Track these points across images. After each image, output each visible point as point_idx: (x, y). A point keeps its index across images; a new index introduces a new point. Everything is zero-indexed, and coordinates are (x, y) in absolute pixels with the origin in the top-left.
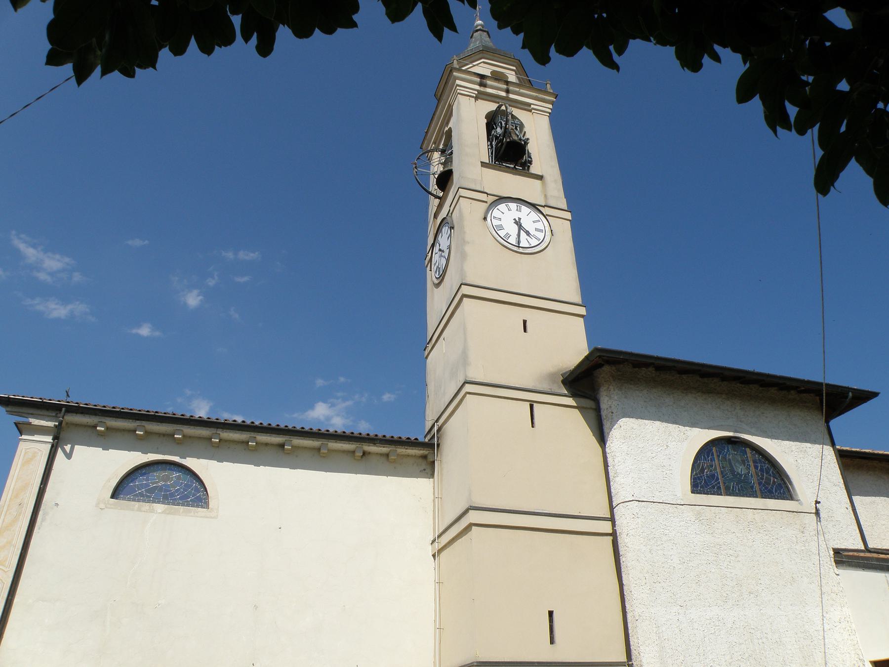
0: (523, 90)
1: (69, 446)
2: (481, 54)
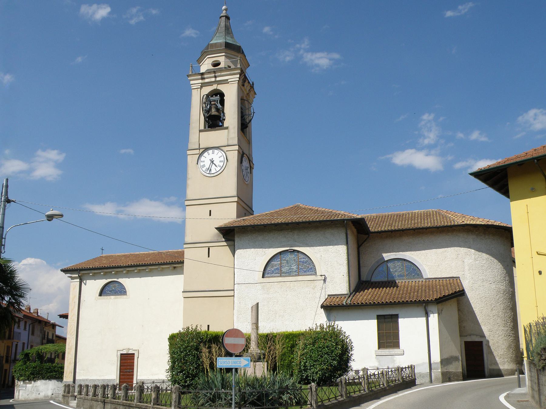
1: (85, 281)
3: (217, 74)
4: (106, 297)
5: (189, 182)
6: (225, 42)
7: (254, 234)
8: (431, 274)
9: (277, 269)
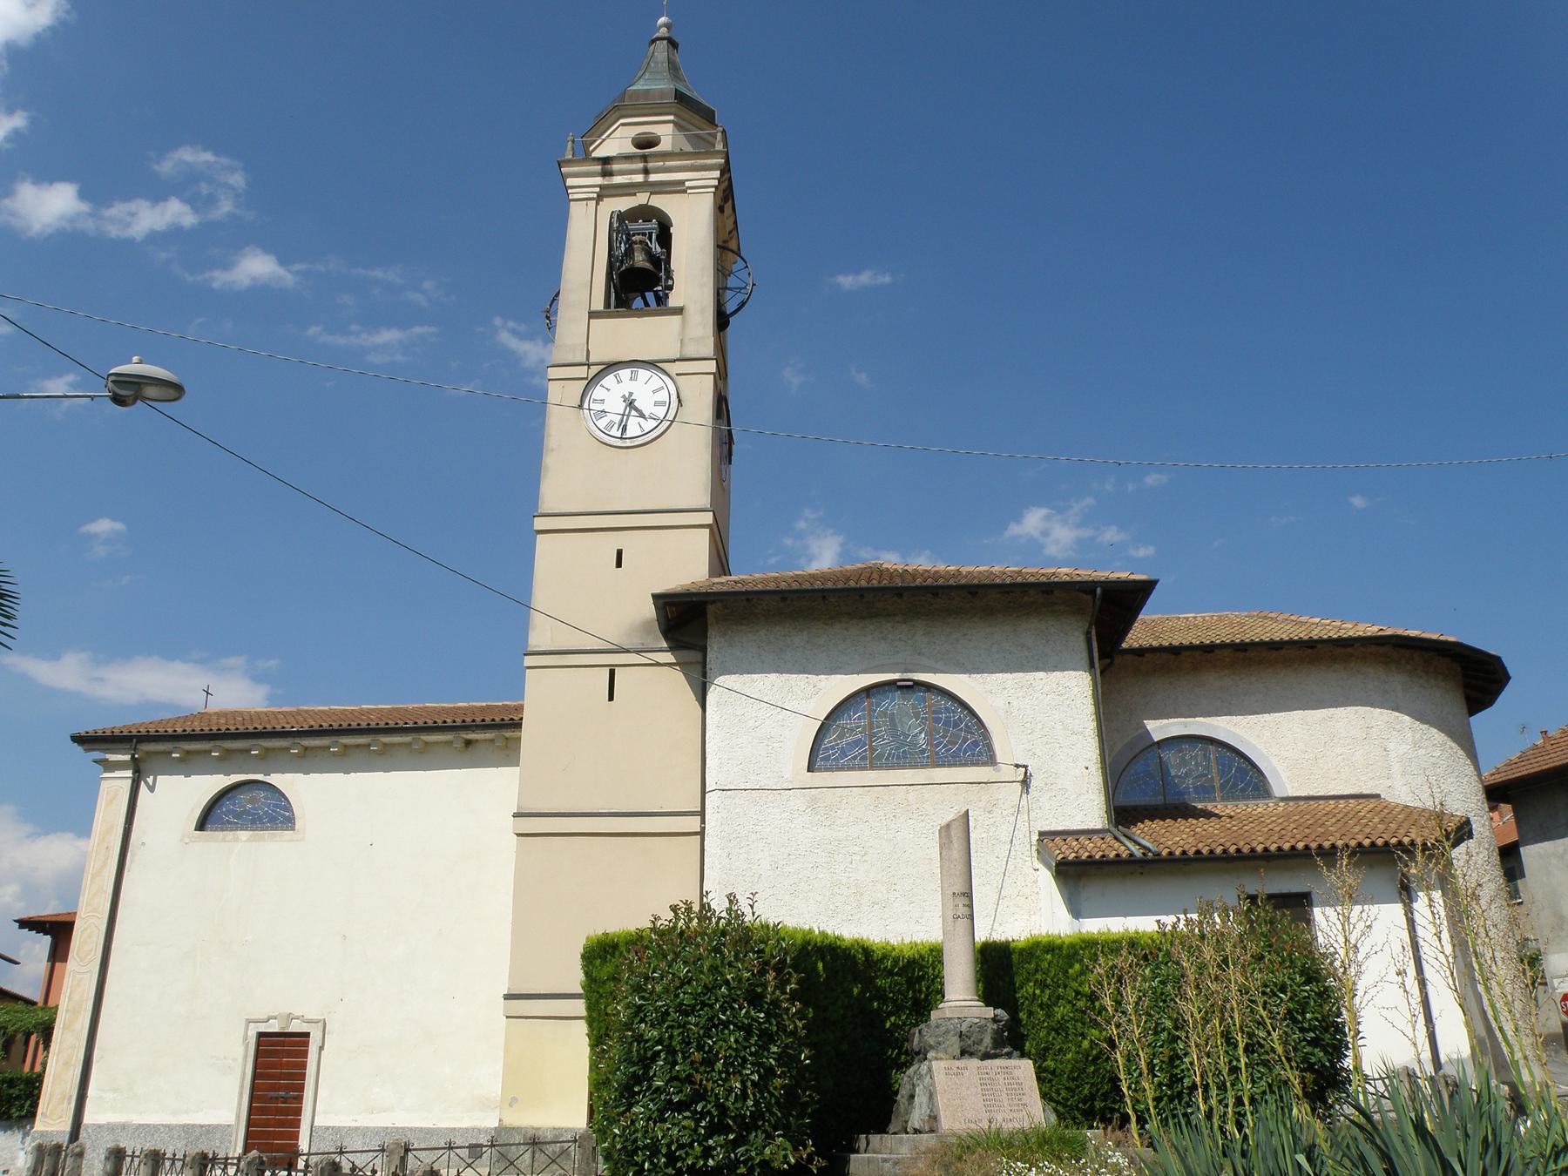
0: (673, 161)
2: (617, 113)
3: (650, 165)
4: (221, 833)
5: (550, 460)
6: (676, 90)
7: (776, 624)
8: (1296, 785)
9: (857, 743)
